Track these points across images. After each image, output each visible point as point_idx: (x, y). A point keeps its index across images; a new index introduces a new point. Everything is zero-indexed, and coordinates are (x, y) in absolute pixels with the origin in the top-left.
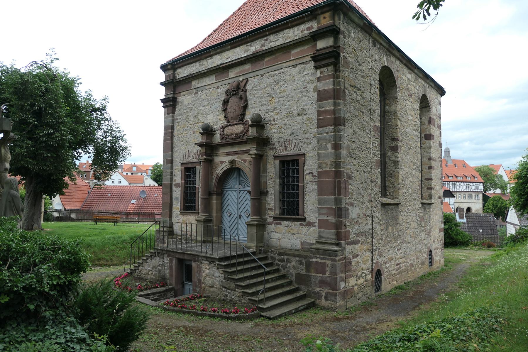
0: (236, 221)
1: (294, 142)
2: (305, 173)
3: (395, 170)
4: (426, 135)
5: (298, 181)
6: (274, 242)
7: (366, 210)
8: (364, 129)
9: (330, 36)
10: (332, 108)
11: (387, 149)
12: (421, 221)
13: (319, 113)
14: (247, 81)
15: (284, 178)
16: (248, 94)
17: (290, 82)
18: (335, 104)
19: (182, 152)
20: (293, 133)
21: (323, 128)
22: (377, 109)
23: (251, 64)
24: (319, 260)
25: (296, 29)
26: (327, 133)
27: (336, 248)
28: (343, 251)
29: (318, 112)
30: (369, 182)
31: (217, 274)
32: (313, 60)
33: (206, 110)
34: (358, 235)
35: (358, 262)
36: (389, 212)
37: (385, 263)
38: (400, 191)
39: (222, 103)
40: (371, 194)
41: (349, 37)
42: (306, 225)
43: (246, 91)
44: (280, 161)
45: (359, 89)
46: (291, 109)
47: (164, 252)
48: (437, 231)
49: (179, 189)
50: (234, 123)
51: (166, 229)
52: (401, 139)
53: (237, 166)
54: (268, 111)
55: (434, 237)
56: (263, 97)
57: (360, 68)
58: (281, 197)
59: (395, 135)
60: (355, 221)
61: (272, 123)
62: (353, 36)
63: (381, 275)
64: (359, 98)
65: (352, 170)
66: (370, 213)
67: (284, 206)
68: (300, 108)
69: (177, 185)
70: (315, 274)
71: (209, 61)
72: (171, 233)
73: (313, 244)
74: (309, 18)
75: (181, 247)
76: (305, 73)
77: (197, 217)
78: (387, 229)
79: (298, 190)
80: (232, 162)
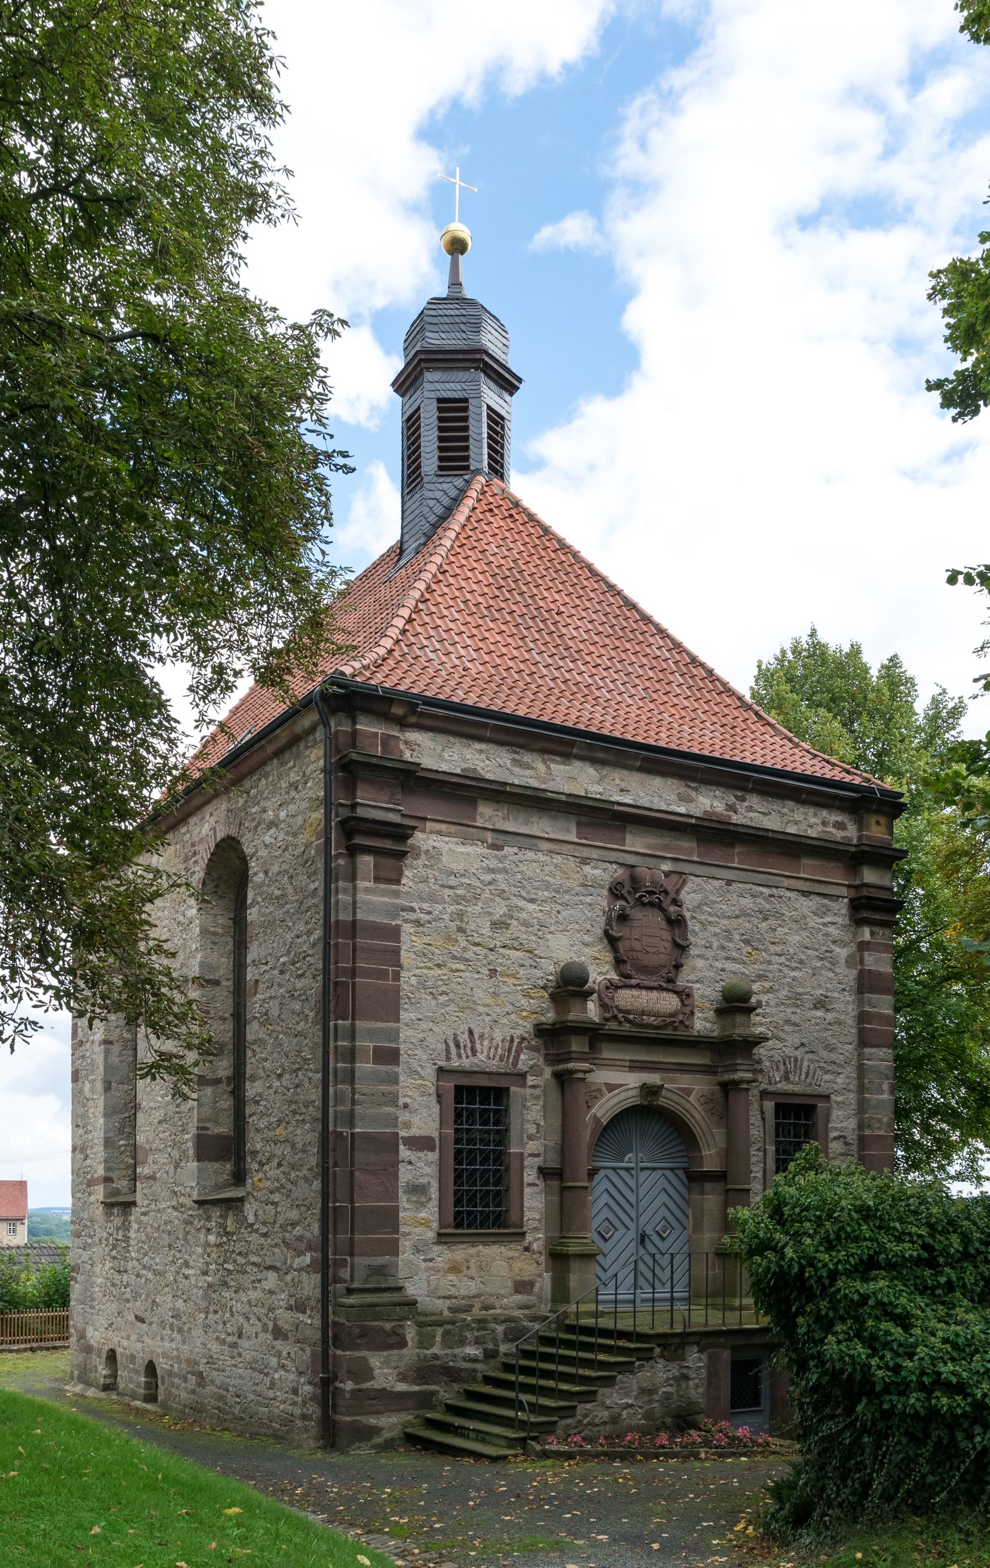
1: (806, 1064)
2: (833, 1134)
17: (795, 926)
25: (811, 810)
26: (882, 1060)
33: (540, 915)
46: (800, 990)
49: (433, 1156)
50: (655, 984)
69: (420, 1143)
76: (829, 919)
80: (650, 1091)
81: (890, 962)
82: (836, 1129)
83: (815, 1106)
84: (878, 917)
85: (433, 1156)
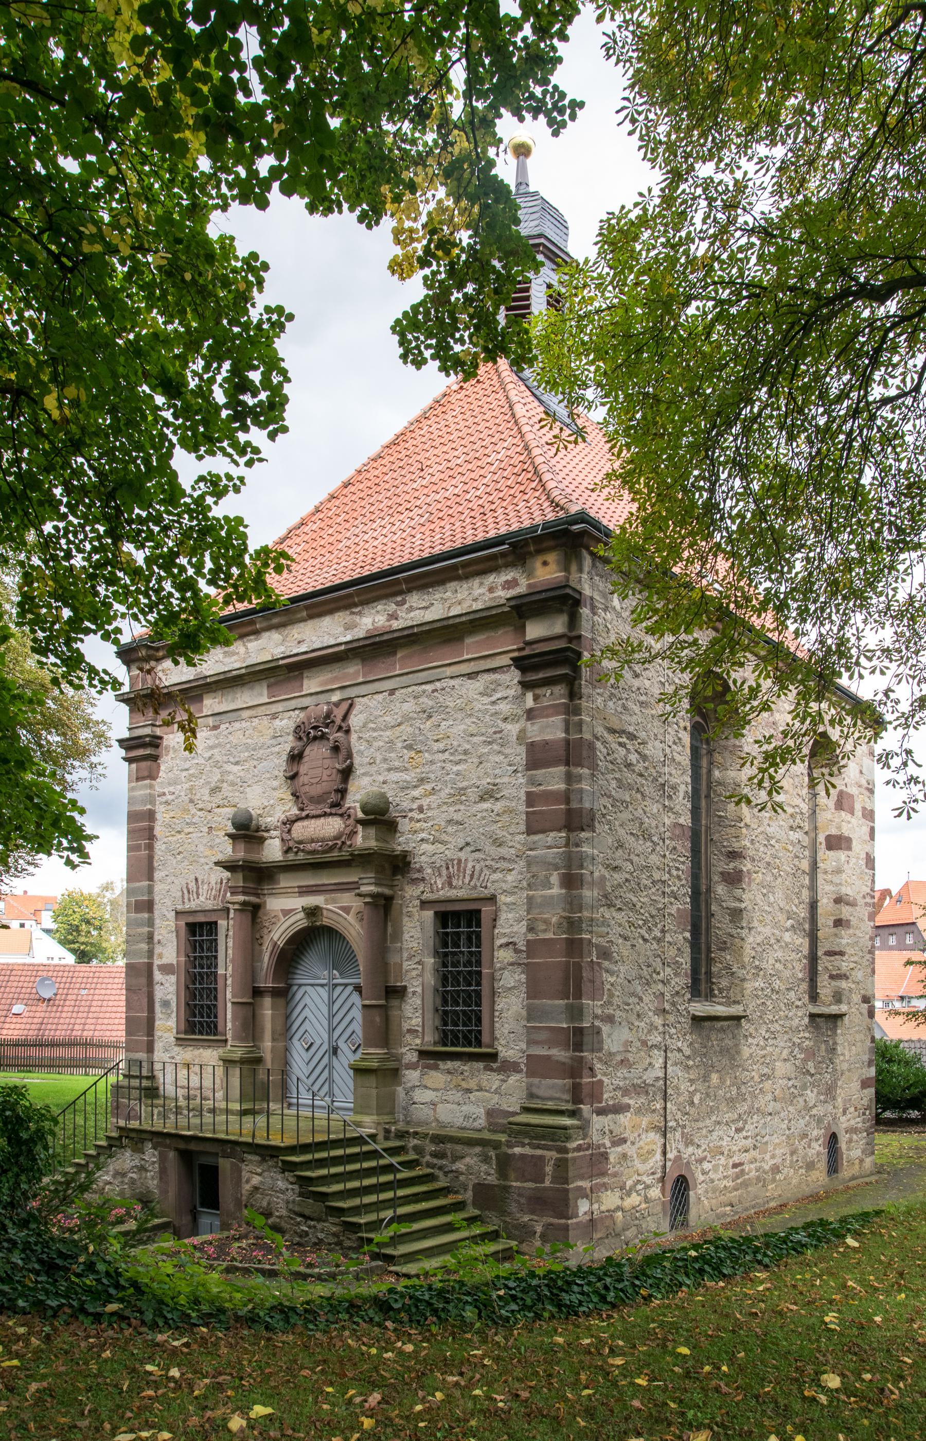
0: (325, 1060)
1: (470, 865)
2: (498, 942)
3: (734, 932)
4: (829, 838)
5: (479, 963)
6: (422, 1113)
7: (649, 1031)
8: (646, 836)
9: (561, 611)
10: (562, 786)
11: (716, 878)
12: (805, 1061)
13: (531, 799)
14: (351, 705)
15: (446, 955)
16: (354, 737)
17: (459, 715)
18: (569, 778)
19: (180, 882)
20: (468, 844)
21: (540, 836)
22: (683, 781)
23: (364, 660)
24: (527, 1151)
25: (476, 582)
26: (549, 847)
27: (567, 1121)
28: (584, 1128)
29: (528, 794)
30: (657, 964)
31: (281, 1184)
32: (517, 667)
33: (242, 774)
34: (626, 1092)
35: (624, 1156)
36: (713, 1037)
37: (700, 1161)
38: (749, 986)
39: (285, 757)
40: (662, 994)
41: (606, 609)
42: (498, 1070)
43: (348, 732)
44: (436, 913)
45: (632, 737)
46: (465, 784)
47: (144, 1136)
48: (856, 1085)
49: (173, 978)
50: (319, 812)
51: (135, 1083)
52: (751, 853)
53: (326, 922)
54: (406, 787)
55: (845, 1101)
56: (391, 749)
57: (636, 683)
58: (439, 1001)
59: (736, 845)
60: (619, 1058)
61: (415, 815)
62: (618, 607)
63: (687, 1188)
64: (633, 758)
65: (611, 937)
66: (659, 1039)
67: (445, 1024)
68: (484, 782)
69: (167, 969)
70: (518, 1184)
71: (249, 645)
72: (152, 1093)
73: (514, 1114)
74: (510, 559)
75: (188, 1125)
76: (499, 695)
77: (221, 1050)
78: (706, 1078)
79: (479, 984)
80: (312, 912)
81: (561, 725)
82: (504, 935)
83: (479, 911)
84: (541, 675)
85: (173, 978)
